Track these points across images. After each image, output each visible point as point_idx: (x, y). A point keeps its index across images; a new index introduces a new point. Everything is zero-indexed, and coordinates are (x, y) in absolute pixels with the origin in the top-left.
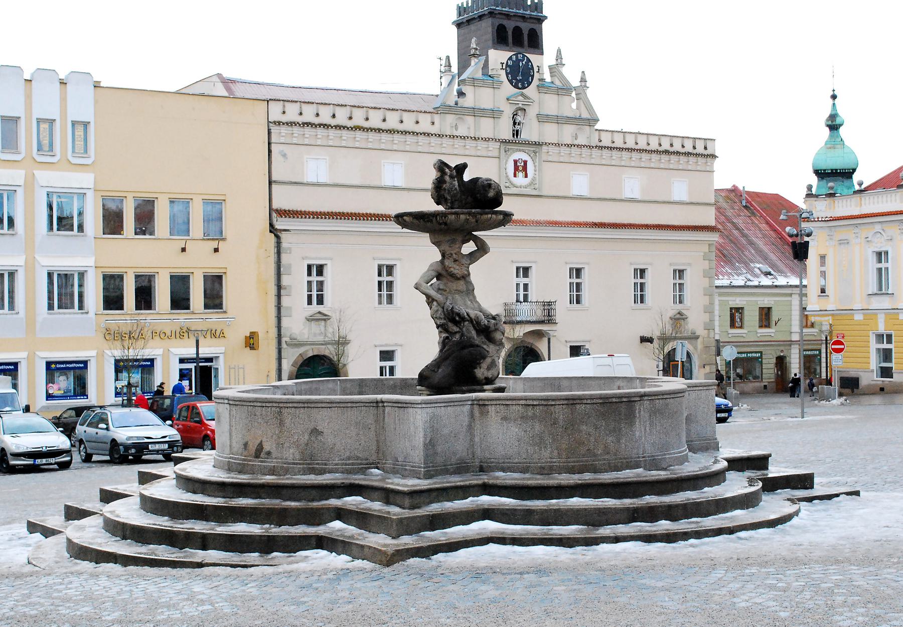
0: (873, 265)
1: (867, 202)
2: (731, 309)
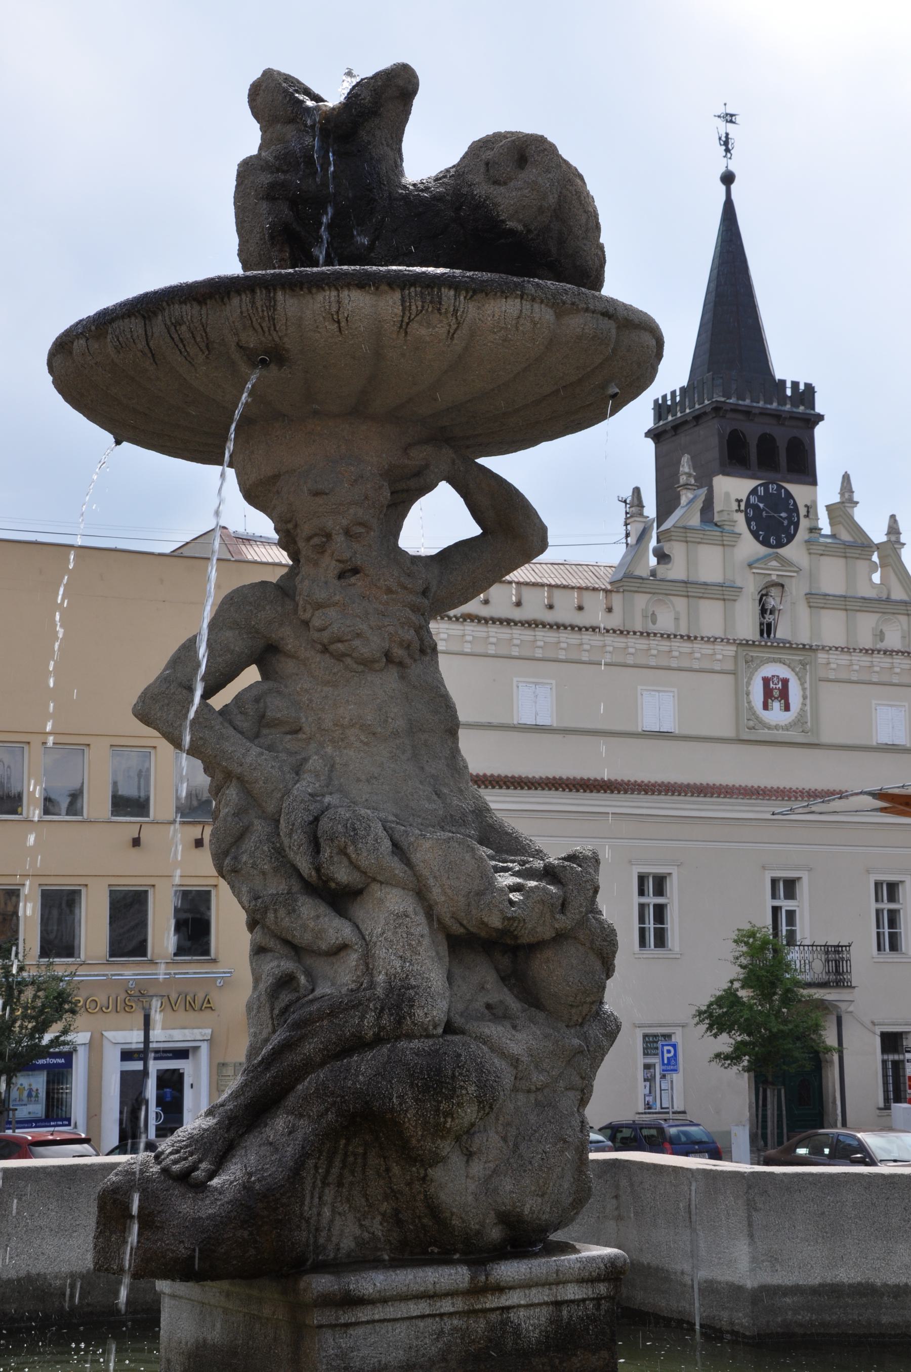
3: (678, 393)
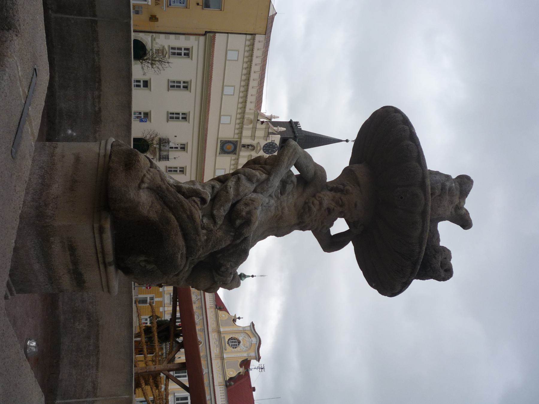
3: (300, 127)
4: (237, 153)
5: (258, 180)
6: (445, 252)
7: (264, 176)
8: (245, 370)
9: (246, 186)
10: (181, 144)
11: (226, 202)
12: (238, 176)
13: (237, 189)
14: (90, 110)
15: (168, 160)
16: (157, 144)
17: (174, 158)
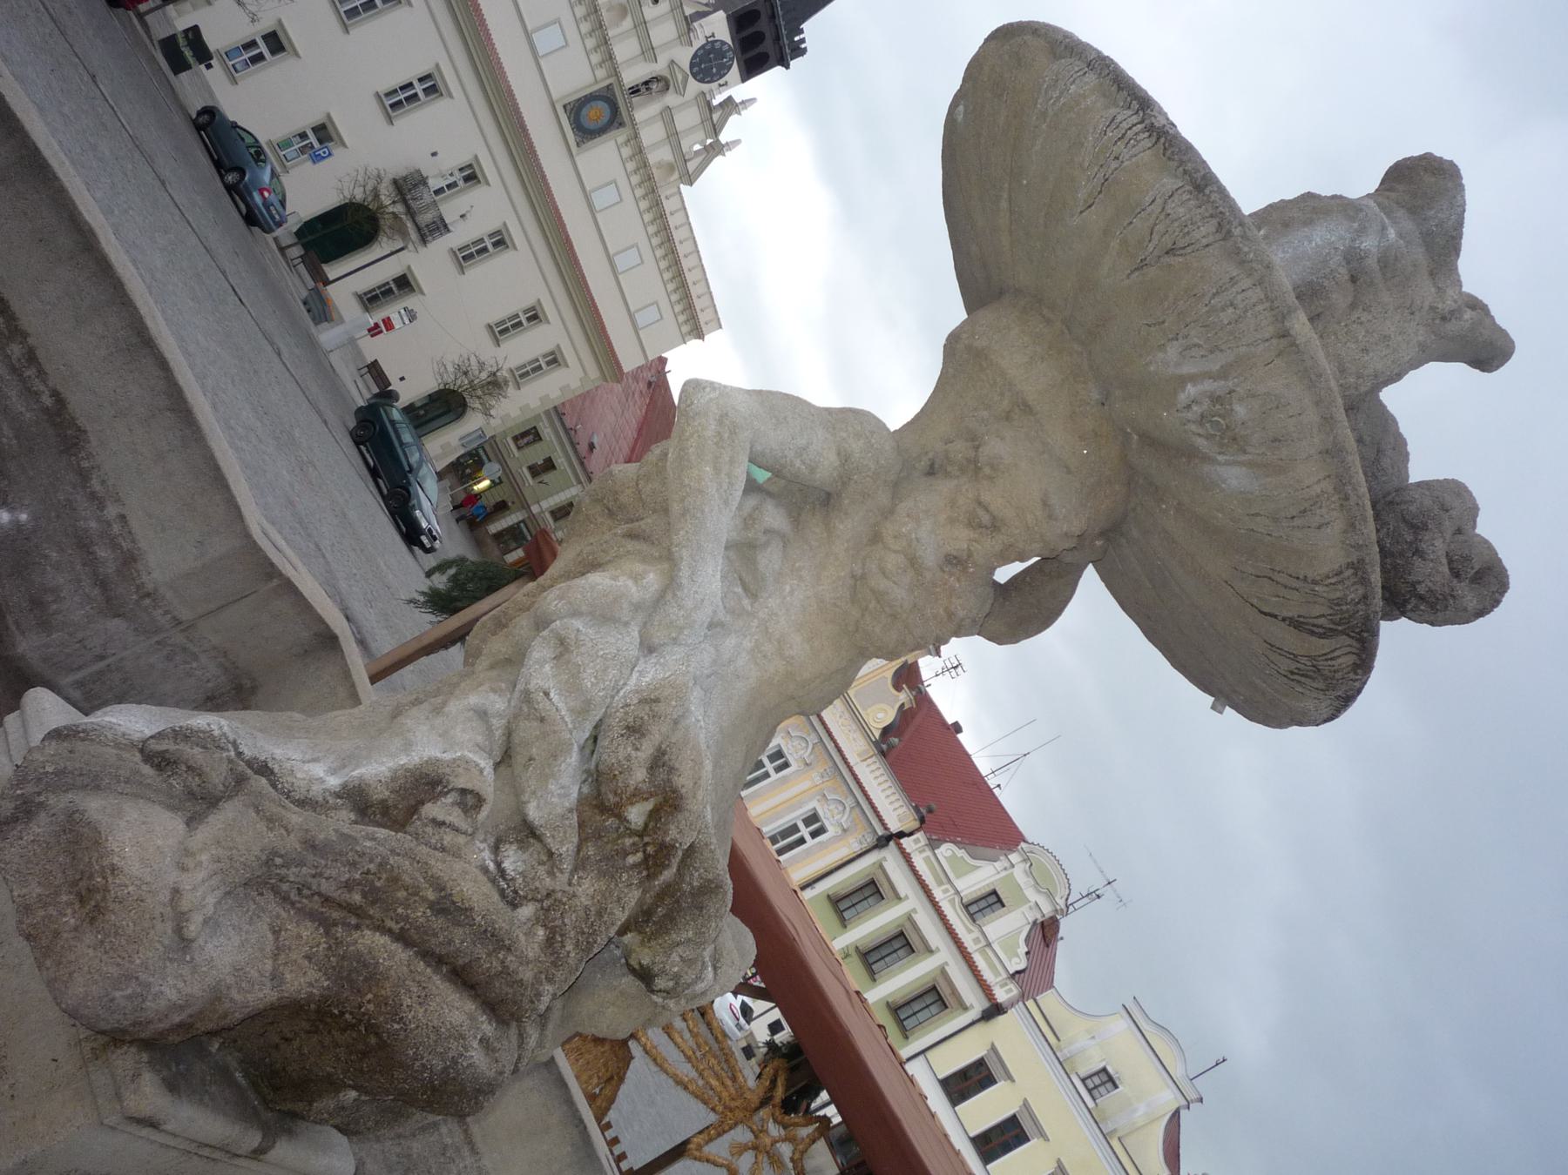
0: (796, 816)
1: (873, 767)
2: (535, 428)
4: (626, 119)
5: (637, 607)
6: (1447, 511)
7: (653, 579)
8: (914, 693)
9: (602, 656)
10: (461, 170)
11: (555, 757)
12: (552, 631)
13: (573, 686)
14: (28, 415)
15: (449, 231)
16: (394, 202)
17: (462, 216)
